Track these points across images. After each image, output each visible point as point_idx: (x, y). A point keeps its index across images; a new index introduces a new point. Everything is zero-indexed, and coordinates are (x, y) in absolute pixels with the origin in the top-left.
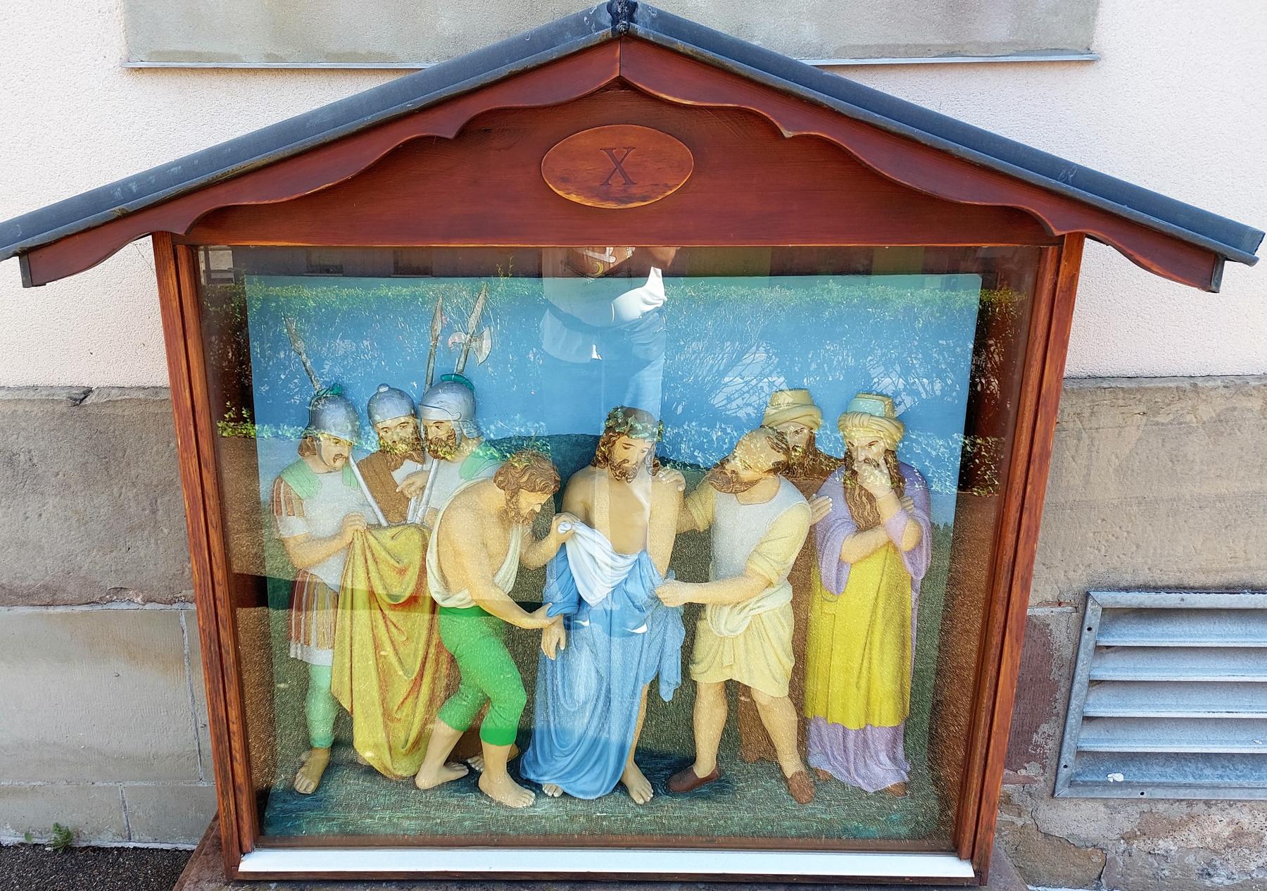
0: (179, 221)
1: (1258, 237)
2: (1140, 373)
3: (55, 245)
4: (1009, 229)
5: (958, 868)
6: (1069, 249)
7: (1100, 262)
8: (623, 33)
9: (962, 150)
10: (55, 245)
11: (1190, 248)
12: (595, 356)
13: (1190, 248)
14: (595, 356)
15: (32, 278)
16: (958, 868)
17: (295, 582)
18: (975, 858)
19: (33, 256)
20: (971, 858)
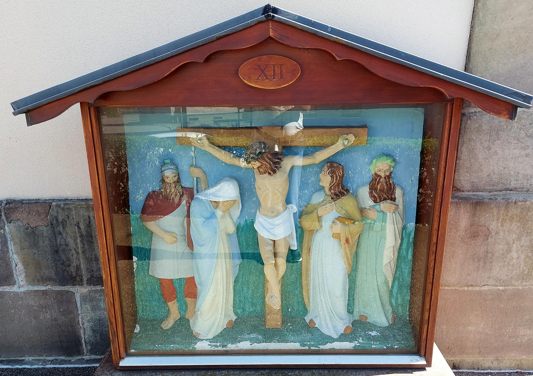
0: (91, 97)
1: (15, 114)
15: (31, 122)
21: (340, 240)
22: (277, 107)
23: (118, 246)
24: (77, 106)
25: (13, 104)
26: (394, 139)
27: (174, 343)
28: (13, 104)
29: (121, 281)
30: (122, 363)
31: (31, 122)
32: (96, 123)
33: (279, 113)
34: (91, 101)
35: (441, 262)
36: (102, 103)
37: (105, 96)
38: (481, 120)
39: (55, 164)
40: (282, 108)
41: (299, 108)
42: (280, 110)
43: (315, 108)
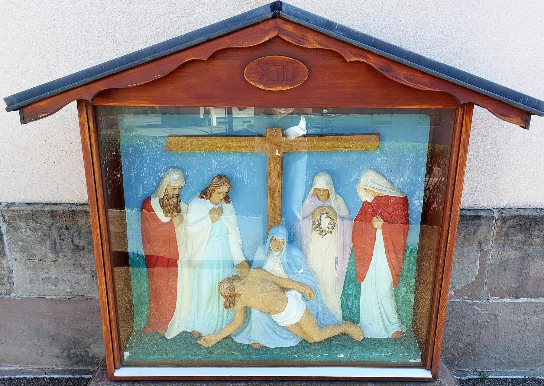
0: (88, 94)
1: (8, 110)
2: (346, 207)
3: (30, 105)
4: (446, 99)
5: (426, 374)
6: (468, 108)
7: (481, 115)
8: (276, 7)
9: (405, 61)
10: (30, 105)
11: (516, 108)
12: (278, 154)
13: (516, 108)
14: (278, 154)
15: (24, 120)
16: (426, 374)
17: (158, 257)
18: (433, 368)
19: (25, 110)
20: (430, 369)
21: (323, 308)
22: (278, 110)
23: (114, 252)
24: (74, 104)
25: (6, 100)
26: (387, 165)
27: (247, 147)
28: (6, 100)
29: (104, 328)
30: (121, 373)
31: (24, 120)
32: (94, 126)
33: (279, 116)
34: (89, 98)
35: (449, 270)
36: (99, 103)
37: (104, 94)
38: (483, 120)
39: (50, 162)
40: (283, 111)
41: (299, 113)
42: (281, 114)
43: (318, 111)
